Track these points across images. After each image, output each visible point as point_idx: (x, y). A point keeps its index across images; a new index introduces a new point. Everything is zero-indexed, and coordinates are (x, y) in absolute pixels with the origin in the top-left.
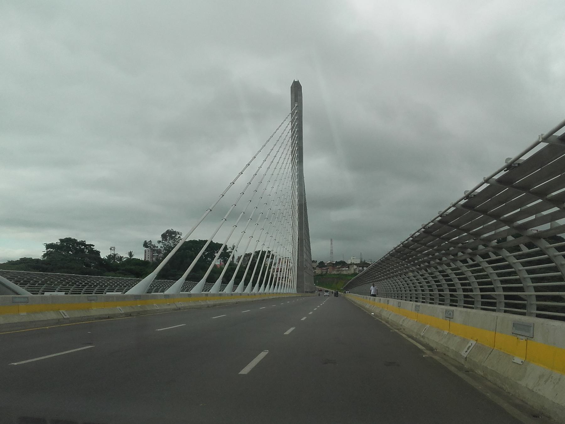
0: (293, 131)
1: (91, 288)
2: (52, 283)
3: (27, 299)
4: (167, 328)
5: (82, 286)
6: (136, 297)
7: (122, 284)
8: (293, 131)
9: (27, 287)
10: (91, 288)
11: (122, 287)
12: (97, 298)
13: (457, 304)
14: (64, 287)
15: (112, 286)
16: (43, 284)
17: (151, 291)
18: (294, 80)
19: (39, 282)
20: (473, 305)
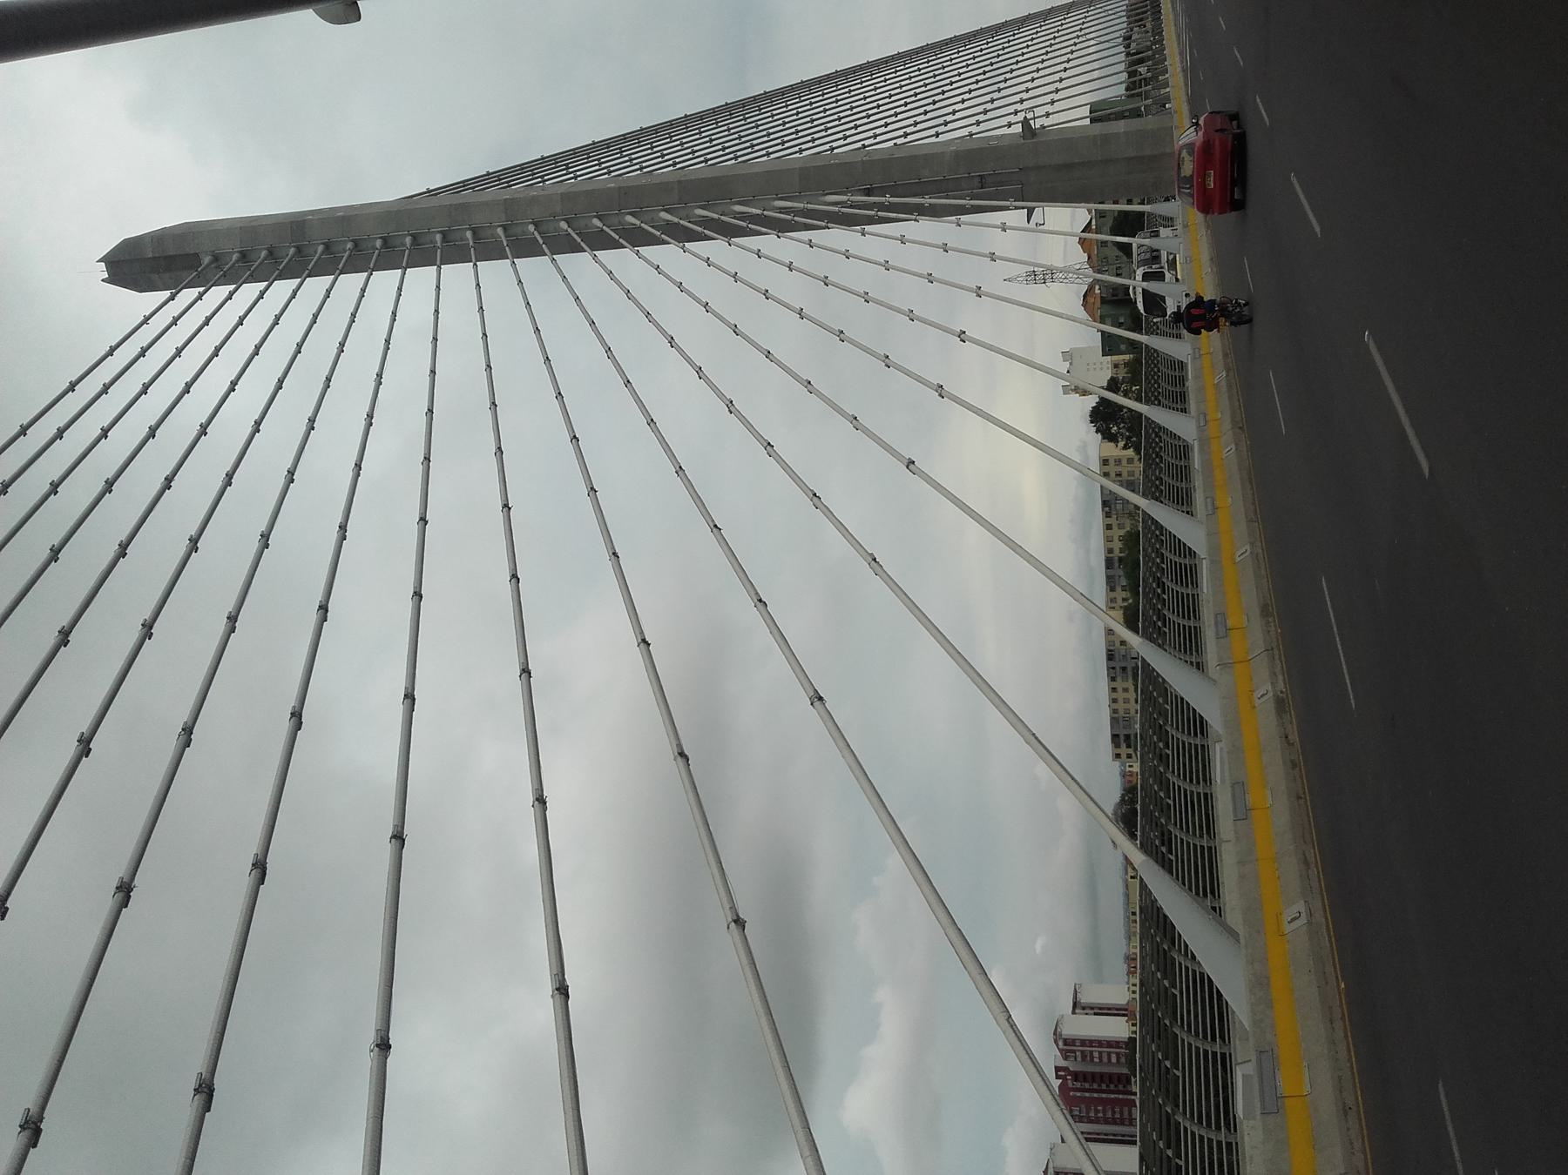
0: (699, 229)
1: (1170, 633)
2: (1163, 754)
3: (1236, 786)
4: (1340, 652)
5: (1172, 854)
6: (1260, 984)
7: (1155, 491)
8: (699, 229)
9: (1198, 840)
10: (1169, 600)
11: (1163, 488)
12: (1238, 783)
13: (1228, 1054)
14: (1169, 603)
15: (1161, 447)
16: (1161, 585)
17: (1170, 536)
18: (1102, 388)
19: (1159, 977)
20: (1225, 1054)
